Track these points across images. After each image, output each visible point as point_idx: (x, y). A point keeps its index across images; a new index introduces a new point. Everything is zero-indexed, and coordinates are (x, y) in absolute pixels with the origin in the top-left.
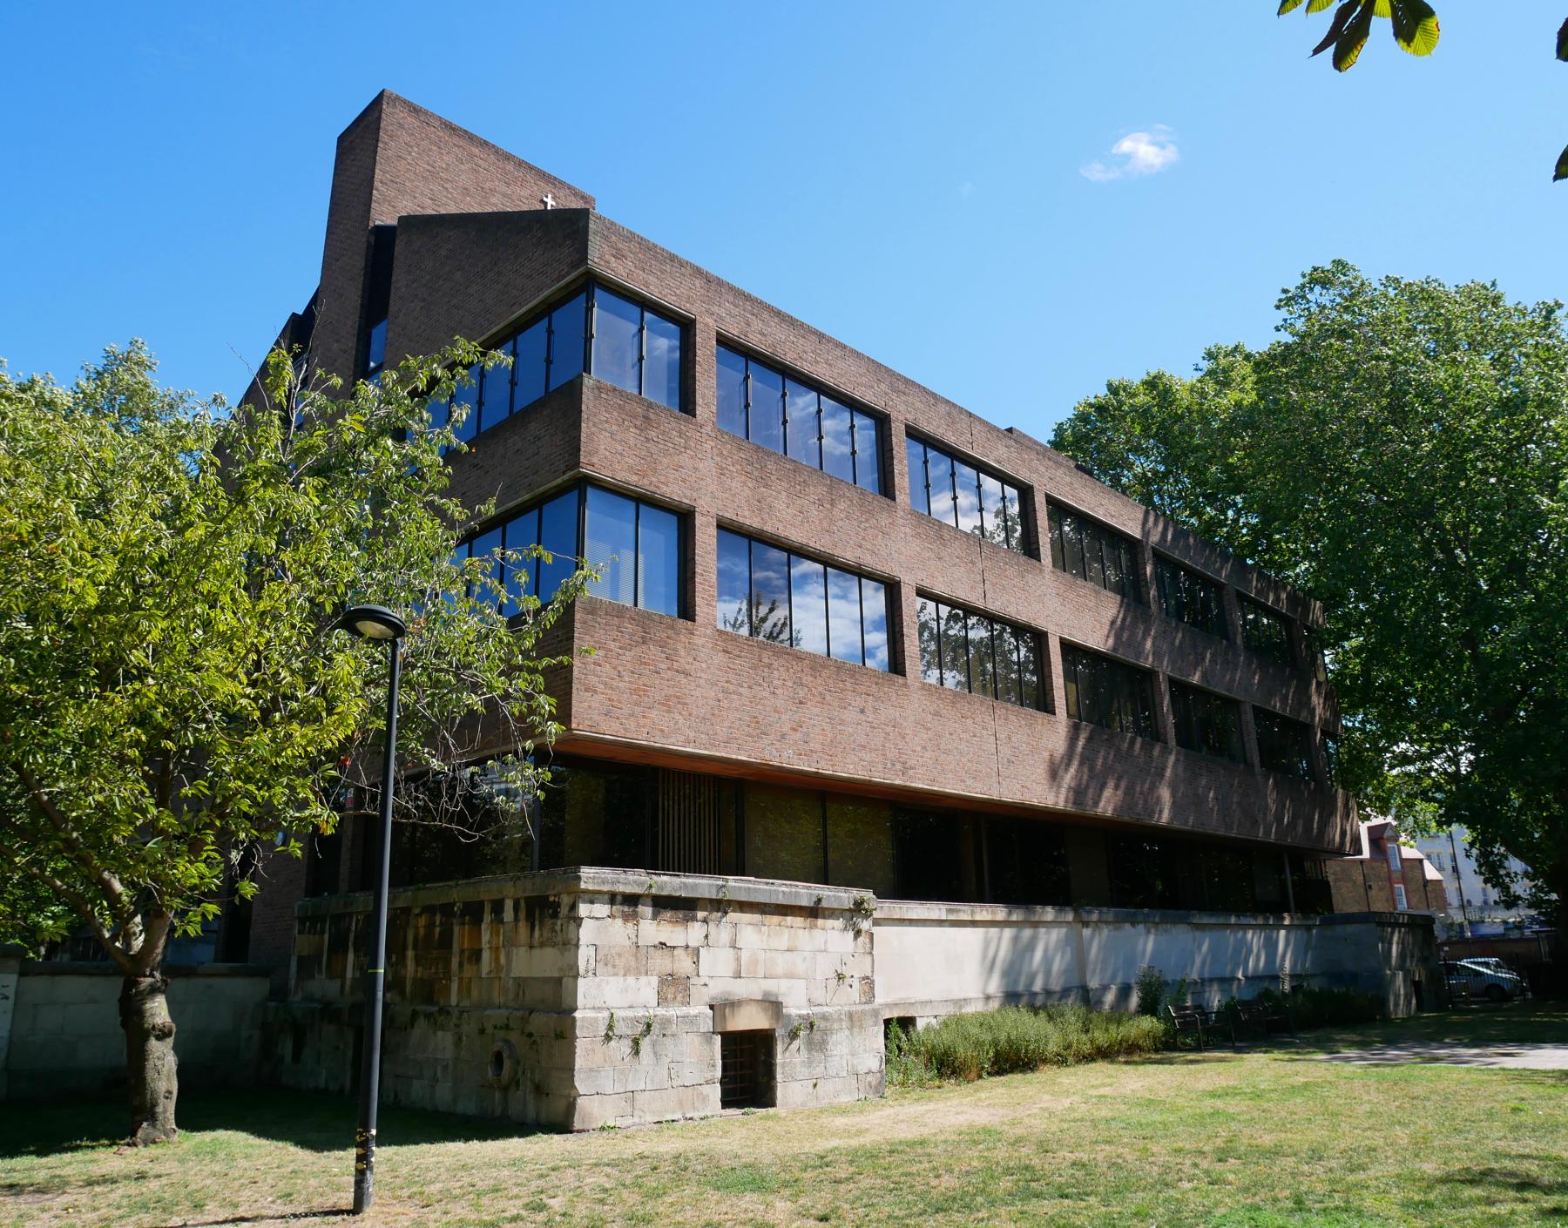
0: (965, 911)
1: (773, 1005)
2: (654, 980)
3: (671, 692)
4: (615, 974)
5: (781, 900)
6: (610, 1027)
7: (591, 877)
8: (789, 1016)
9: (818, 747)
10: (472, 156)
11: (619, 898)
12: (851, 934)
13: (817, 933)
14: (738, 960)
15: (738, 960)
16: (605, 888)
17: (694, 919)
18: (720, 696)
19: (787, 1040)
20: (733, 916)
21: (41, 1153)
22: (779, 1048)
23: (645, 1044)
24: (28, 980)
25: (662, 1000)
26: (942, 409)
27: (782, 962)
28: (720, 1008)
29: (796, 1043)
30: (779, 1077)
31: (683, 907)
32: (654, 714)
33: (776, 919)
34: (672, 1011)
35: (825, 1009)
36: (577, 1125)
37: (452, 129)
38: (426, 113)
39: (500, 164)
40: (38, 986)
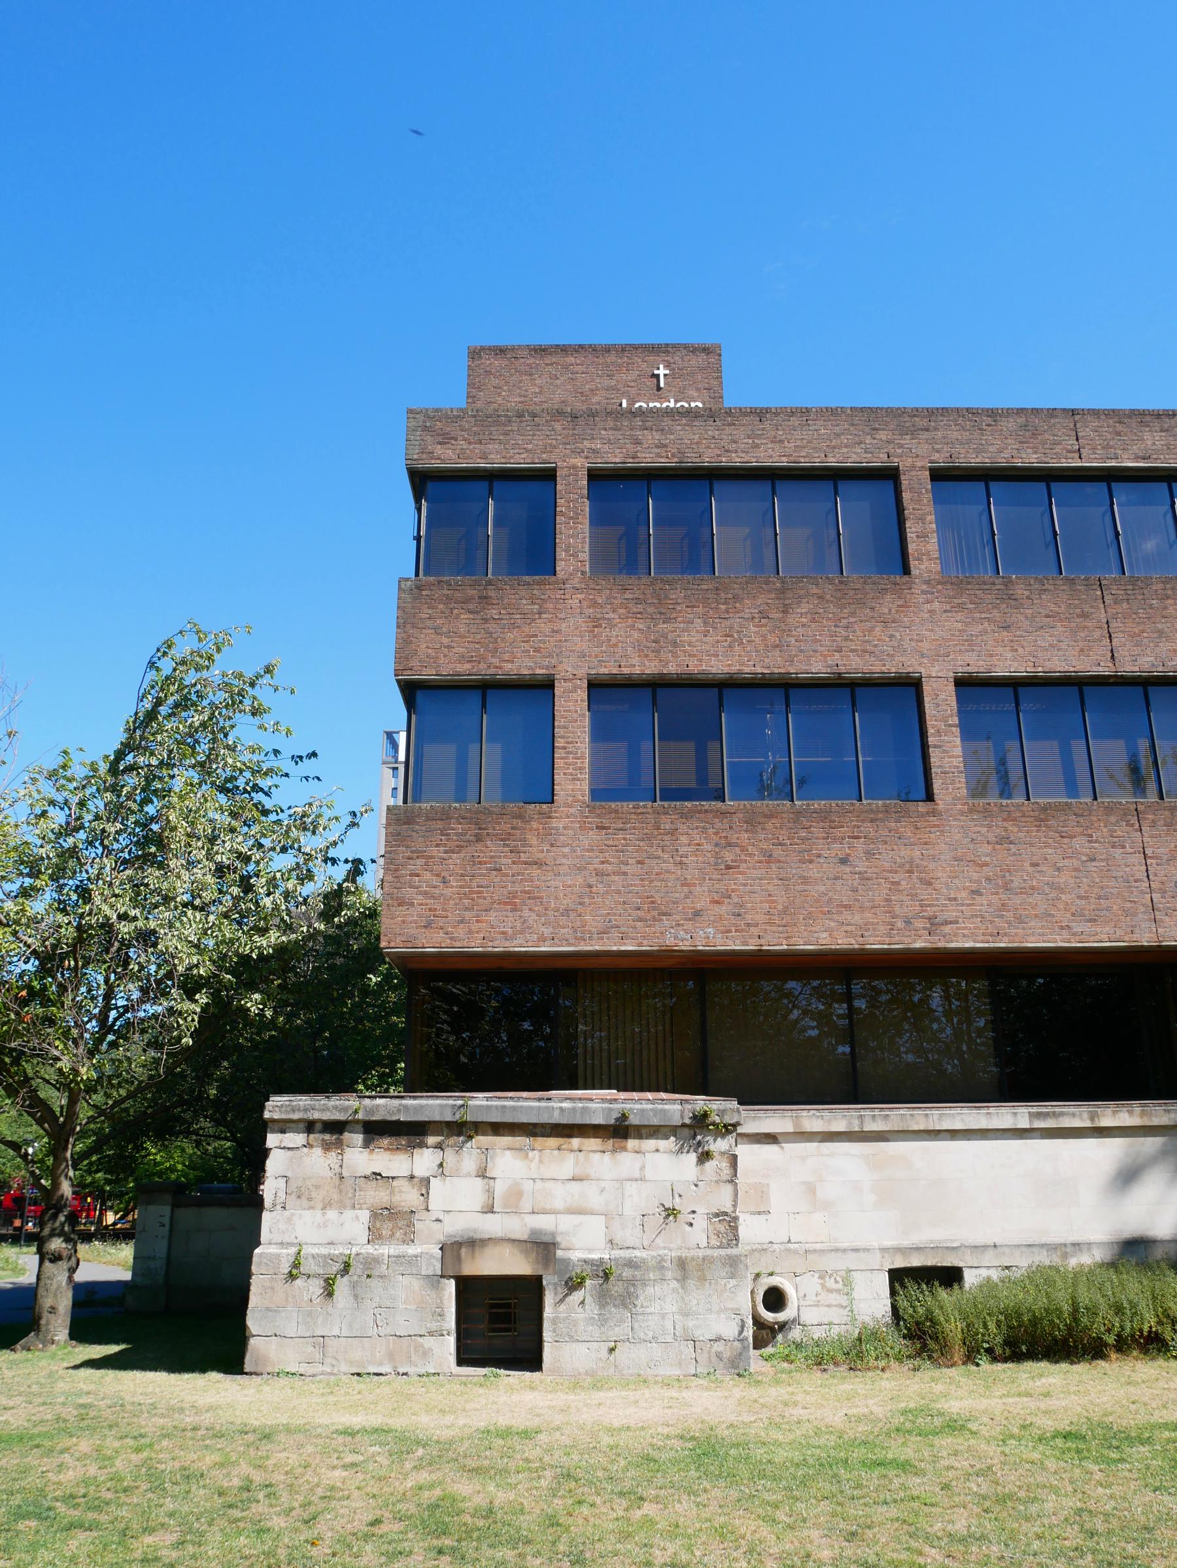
0: (1075, 1114)
1: (543, 1247)
2: (365, 1215)
3: (518, 888)
4: (312, 1208)
5: (556, 1118)
6: (296, 1265)
7: (277, 1106)
8: (566, 1262)
9: (761, 918)
10: (566, 367)
11: (319, 1126)
12: (693, 1157)
13: (623, 1157)
14: (490, 1192)
15: (490, 1192)
16: (296, 1116)
17: (422, 1145)
18: (593, 880)
19: (562, 1291)
20: (481, 1140)
21: (506, 1369)
22: (549, 1299)
23: (342, 1285)
24: (180, 1212)
25: (374, 1235)
26: (1010, 424)
27: (561, 1195)
28: (453, 1249)
29: (577, 1296)
30: (547, 1335)
31: (411, 1132)
32: (492, 917)
33: (553, 1142)
34: (385, 1250)
35: (637, 1253)
36: (248, 1367)
37: (541, 351)
38: (513, 349)
39: (601, 360)
40: (187, 1215)
